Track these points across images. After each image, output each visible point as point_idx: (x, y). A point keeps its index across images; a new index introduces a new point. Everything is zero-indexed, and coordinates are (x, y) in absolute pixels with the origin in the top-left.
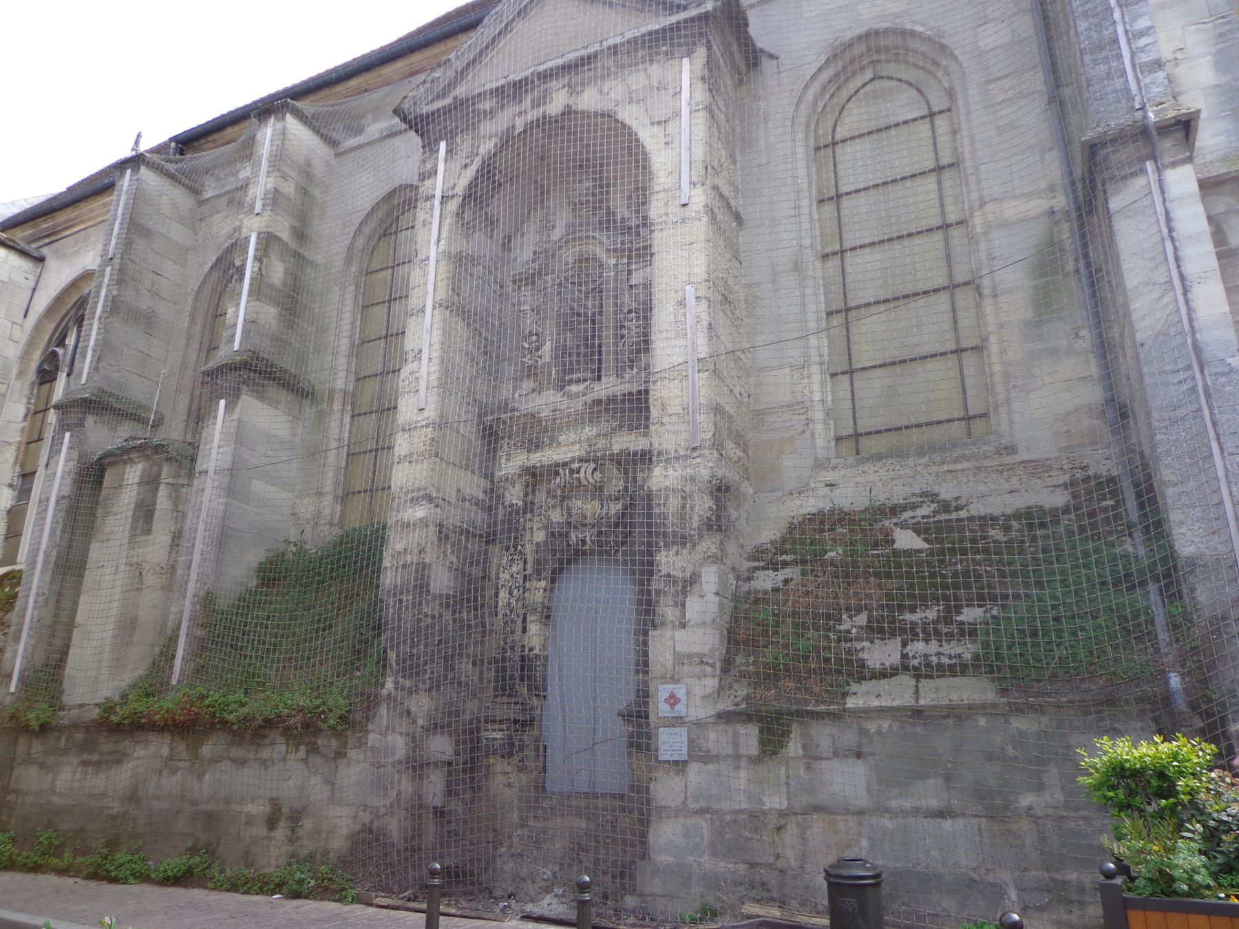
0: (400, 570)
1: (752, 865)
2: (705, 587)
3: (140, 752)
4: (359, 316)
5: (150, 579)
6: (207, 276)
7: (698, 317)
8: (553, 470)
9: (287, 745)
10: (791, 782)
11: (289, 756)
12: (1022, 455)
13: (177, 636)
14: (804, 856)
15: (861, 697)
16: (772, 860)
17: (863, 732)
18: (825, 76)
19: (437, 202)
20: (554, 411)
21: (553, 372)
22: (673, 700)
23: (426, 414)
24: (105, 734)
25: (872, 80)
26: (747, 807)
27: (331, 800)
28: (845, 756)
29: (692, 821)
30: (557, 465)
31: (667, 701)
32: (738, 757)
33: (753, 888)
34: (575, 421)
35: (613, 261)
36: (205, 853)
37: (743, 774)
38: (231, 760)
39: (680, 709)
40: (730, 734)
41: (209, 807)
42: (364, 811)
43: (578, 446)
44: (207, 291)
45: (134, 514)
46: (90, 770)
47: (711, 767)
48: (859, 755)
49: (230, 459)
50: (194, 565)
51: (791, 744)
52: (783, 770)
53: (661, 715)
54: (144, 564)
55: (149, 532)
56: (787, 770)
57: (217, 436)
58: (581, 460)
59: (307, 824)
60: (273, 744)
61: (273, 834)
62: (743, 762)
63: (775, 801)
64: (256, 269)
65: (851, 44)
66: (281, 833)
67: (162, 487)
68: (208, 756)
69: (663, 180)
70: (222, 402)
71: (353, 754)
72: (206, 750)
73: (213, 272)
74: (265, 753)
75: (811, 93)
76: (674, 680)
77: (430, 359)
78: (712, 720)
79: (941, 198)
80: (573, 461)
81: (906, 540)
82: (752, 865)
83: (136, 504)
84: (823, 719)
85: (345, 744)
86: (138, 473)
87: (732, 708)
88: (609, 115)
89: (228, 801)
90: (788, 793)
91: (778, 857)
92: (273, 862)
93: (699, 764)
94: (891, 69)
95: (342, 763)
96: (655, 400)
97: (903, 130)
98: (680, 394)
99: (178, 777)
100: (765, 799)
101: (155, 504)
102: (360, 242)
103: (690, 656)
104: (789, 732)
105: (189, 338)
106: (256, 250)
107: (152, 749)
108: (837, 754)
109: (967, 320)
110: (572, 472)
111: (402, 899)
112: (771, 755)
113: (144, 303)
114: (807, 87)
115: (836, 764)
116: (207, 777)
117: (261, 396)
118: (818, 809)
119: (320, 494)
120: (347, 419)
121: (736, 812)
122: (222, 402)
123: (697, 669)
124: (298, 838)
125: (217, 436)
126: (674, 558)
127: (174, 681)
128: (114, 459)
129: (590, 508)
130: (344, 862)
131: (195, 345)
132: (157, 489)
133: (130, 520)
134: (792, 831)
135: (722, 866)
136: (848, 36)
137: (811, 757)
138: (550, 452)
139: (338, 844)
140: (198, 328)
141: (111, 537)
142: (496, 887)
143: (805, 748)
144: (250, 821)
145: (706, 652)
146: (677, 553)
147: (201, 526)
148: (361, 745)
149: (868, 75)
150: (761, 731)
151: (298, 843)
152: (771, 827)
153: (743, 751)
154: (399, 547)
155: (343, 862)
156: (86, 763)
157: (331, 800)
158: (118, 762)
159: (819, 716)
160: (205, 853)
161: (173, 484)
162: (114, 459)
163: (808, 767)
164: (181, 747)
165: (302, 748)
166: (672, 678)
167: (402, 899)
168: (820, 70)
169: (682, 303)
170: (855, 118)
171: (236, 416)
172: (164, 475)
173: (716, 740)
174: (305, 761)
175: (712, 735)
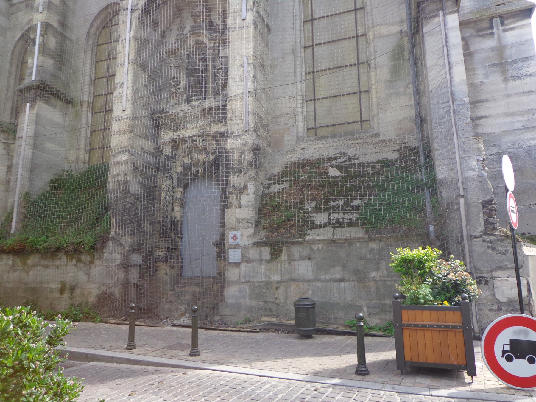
0: (116, 183)
1: (266, 302)
2: (249, 191)
4: (94, 66)
8: (185, 140)
9: (67, 259)
11: (68, 264)
12: (382, 138)
13: (13, 212)
15: (312, 235)
17: (311, 249)
20: (185, 113)
22: (235, 238)
23: (126, 113)
32: (261, 260)
33: (266, 311)
34: (194, 119)
37: (263, 267)
38: (41, 266)
39: (238, 241)
40: (258, 251)
41: (33, 286)
42: (103, 285)
44: (17, 51)
47: (250, 264)
48: (310, 259)
50: (19, 180)
51: (283, 255)
52: (279, 265)
56: (281, 265)
58: (196, 136)
59: (78, 291)
62: (263, 262)
63: (276, 277)
64: (41, 40)
66: (66, 295)
70: (28, 105)
71: (97, 262)
72: (30, 261)
74: (57, 262)
77: (127, 87)
78: (251, 245)
82: (266, 302)
84: (296, 244)
89: (41, 283)
90: (281, 274)
91: (276, 299)
95: (92, 266)
96: (229, 109)
98: (240, 107)
99: (17, 273)
102: (93, 30)
103: (242, 220)
104: (282, 250)
105: (10, 73)
106: (41, 31)
108: (301, 258)
111: (121, 320)
115: (301, 262)
116: (31, 273)
118: (293, 280)
120: (90, 114)
122: (28, 105)
123: (245, 225)
124: (74, 297)
135: (254, 303)
137: (291, 259)
139: (92, 299)
140: (14, 69)
143: (288, 256)
144: (52, 291)
145: (249, 218)
146: (238, 177)
147: (21, 163)
148: (101, 258)
150: (271, 250)
151: (74, 299)
153: (263, 258)
154: (115, 173)
157: (88, 281)
163: (289, 264)
164: (18, 260)
165: (74, 260)
166: (235, 228)
167: (121, 320)
171: (35, 111)
173: (252, 253)
174: (76, 265)
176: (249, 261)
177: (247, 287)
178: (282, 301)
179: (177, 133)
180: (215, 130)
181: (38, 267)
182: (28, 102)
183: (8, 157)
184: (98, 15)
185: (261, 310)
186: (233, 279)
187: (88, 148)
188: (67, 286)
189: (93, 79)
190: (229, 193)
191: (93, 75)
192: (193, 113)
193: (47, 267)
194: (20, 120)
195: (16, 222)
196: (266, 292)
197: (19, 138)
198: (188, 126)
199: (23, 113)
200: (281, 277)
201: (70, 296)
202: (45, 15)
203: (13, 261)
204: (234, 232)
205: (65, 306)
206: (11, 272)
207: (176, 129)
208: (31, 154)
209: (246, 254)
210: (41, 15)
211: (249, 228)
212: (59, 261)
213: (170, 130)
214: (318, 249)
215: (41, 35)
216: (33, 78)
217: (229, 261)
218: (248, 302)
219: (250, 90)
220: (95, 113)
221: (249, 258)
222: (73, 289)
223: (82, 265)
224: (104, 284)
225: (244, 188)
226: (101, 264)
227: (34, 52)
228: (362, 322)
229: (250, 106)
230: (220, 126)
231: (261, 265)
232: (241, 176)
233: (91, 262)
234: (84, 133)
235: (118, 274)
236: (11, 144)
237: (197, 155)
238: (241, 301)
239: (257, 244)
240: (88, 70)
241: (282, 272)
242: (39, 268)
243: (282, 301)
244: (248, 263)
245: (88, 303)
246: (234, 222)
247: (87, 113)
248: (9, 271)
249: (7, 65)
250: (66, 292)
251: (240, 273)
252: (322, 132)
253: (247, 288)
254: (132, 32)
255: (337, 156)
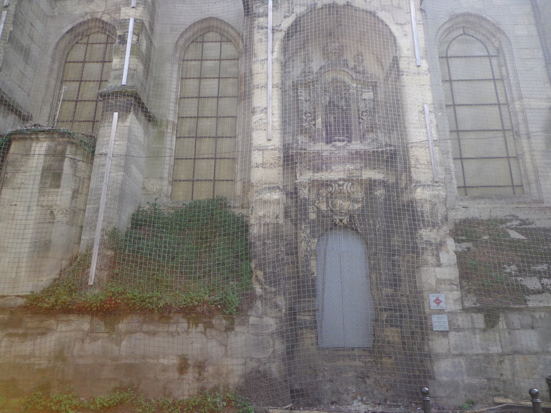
0: (262, 226)
1: (489, 379)
2: (449, 247)
3: (62, 327)
4: (180, 83)
5: (59, 217)
6: (63, 36)
7: (431, 120)
8: (327, 184)
9: (189, 323)
10: (502, 340)
11: (190, 330)
12: (546, 205)
13: (91, 255)
14: (514, 375)
15: (533, 302)
16: (499, 376)
17: (533, 317)
18: (446, 26)
19: (270, 32)
20: (331, 153)
21: (324, 134)
22: (438, 301)
23: (272, 143)
24: (30, 315)
25: (461, 35)
26: (482, 352)
27: (226, 355)
28: (526, 328)
29: (456, 360)
30: (331, 181)
31: (441, 301)
32: (474, 329)
33: (490, 390)
34: (343, 161)
35: (355, 85)
36: (131, 390)
37: (478, 336)
38: (144, 332)
39: (442, 305)
40: (469, 318)
41: (128, 361)
42: (251, 360)
43: (343, 173)
44: (62, 46)
45: (42, 174)
46: (17, 339)
47: (461, 333)
48: (533, 328)
49: (125, 149)
50: (101, 210)
51: (500, 323)
52: (498, 334)
53: (432, 308)
54: (54, 207)
55: (58, 186)
56: (500, 335)
57: (113, 134)
58: (344, 180)
59: (210, 369)
60: (177, 322)
61: (184, 377)
62: (477, 331)
63: (495, 349)
64: (135, 39)
65: (458, 16)
66: (191, 375)
67: (66, 159)
68: (124, 330)
69: (406, 52)
70: (116, 114)
71: (238, 329)
72: (122, 326)
73: (68, 35)
74: (172, 328)
75: (441, 32)
76: (436, 291)
77: (273, 114)
78: (459, 311)
79: (496, 91)
80: (340, 180)
81: (514, 235)
82: (489, 379)
83: (44, 167)
84: (514, 311)
85: (233, 323)
86: (44, 148)
87: (473, 306)
88: (373, 14)
89: (144, 357)
90: (501, 345)
91: (502, 375)
92: (186, 393)
93: (454, 332)
94: (471, 32)
95: (231, 334)
96: (412, 156)
97: (479, 59)
98: (425, 155)
99: (99, 343)
100: (490, 348)
101: (62, 170)
102: (181, 42)
103: (444, 280)
104: (499, 317)
105: (51, 70)
106: (134, 28)
107: (73, 326)
108: (523, 327)
109: (511, 145)
110: (339, 185)
111: (286, 409)
112: (491, 328)
113: (25, 42)
114: (439, 29)
115: (522, 332)
116: (124, 343)
117: (136, 115)
118: (515, 352)
119: (162, 178)
120: (174, 139)
121: (477, 355)
122: (116, 114)
123: (449, 287)
124: (204, 378)
125: (113, 134)
126: (429, 233)
127: (91, 283)
128: (24, 136)
129: (346, 205)
130: (240, 390)
131: (55, 76)
132: (63, 160)
133: (39, 178)
134: (507, 362)
135: (475, 381)
136: (458, 12)
137: (511, 328)
138: (327, 174)
139: (235, 380)
140: (56, 66)
141: (22, 186)
142: (323, 398)
143: (507, 324)
144: (165, 369)
145: (453, 279)
146: (431, 231)
147: (105, 188)
148: (244, 323)
149: (461, 32)
150: (485, 317)
151: (205, 381)
152: (496, 361)
153: (477, 326)
154: (261, 213)
155: (241, 390)
156: (10, 335)
157: (226, 355)
158: (43, 334)
159: (513, 310)
160: (131, 390)
161: (74, 159)
162: (24, 136)
163: (510, 333)
164: (100, 325)
165: (201, 325)
166: (436, 290)
167: (286, 409)
168: (445, 23)
169: (423, 112)
170: (455, 49)
171: (127, 124)
172: (67, 152)
173: (462, 320)
174: (204, 333)
175: (460, 318)
176: (458, 329)
177: (462, 361)
178: (510, 377)
179: (318, 174)
180: (368, 176)
181: (138, 334)
182: (116, 111)
183: (74, 178)
184: (190, 27)
185: (485, 389)
186: (441, 352)
187: (171, 179)
188: (189, 362)
189: (179, 97)
190: (423, 249)
191: (179, 94)
192: (342, 154)
193: (154, 334)
194: (101, 131)
195: (97, 269)
196: (487, 367)
197: (101, 154)
198: (333, 168)
199: (107, 124)
200: (502, 348)
201: (197, 375)
202: (140, 11)
203: (91, 323)
204: (437, 295)
205: (189, 391)
206: (87, 341)
207: (318, 169)
208: (120, 178)
209: (455, 321)
210: (134, 10)
211: (454, 290)
212: (175, 326)
213: (309, 169)
214: (540, 317)
215: (134, 33)
216: (124, 82)
217: (434, 330)
218: (467, 380)
219: (435, 139)
220: (180, 137)
221: (459, 326)
222: (201, 366)
223: (214, 333)
224: (252, 359)
225: (441, 245)
226: (246, 331)
227: (124, 52)
228: (538, 398)
229: (437, 156)
230: (372, 173)
231: (475, 334)
232: (435, 231)
233: (229, 329)
234: (168, 161)
235: (274, 345)
236: (79, 161)
237: (341, 201)
238: (456, 379)
239: (466, 310)
240: (174, 86)
241: (503, 343)
242: (138, 335)
243: (510, 377)
244: (458, 332)
245: (228, 386)
246: (435, 283)
247: (172, 136)
248: (83, 341)
249: (48, 60)
250: (190, 370)
251: (449, 344)
252: (471, 191)
253: (463, 362)
254: (275, 53)
255: (508, 218)
